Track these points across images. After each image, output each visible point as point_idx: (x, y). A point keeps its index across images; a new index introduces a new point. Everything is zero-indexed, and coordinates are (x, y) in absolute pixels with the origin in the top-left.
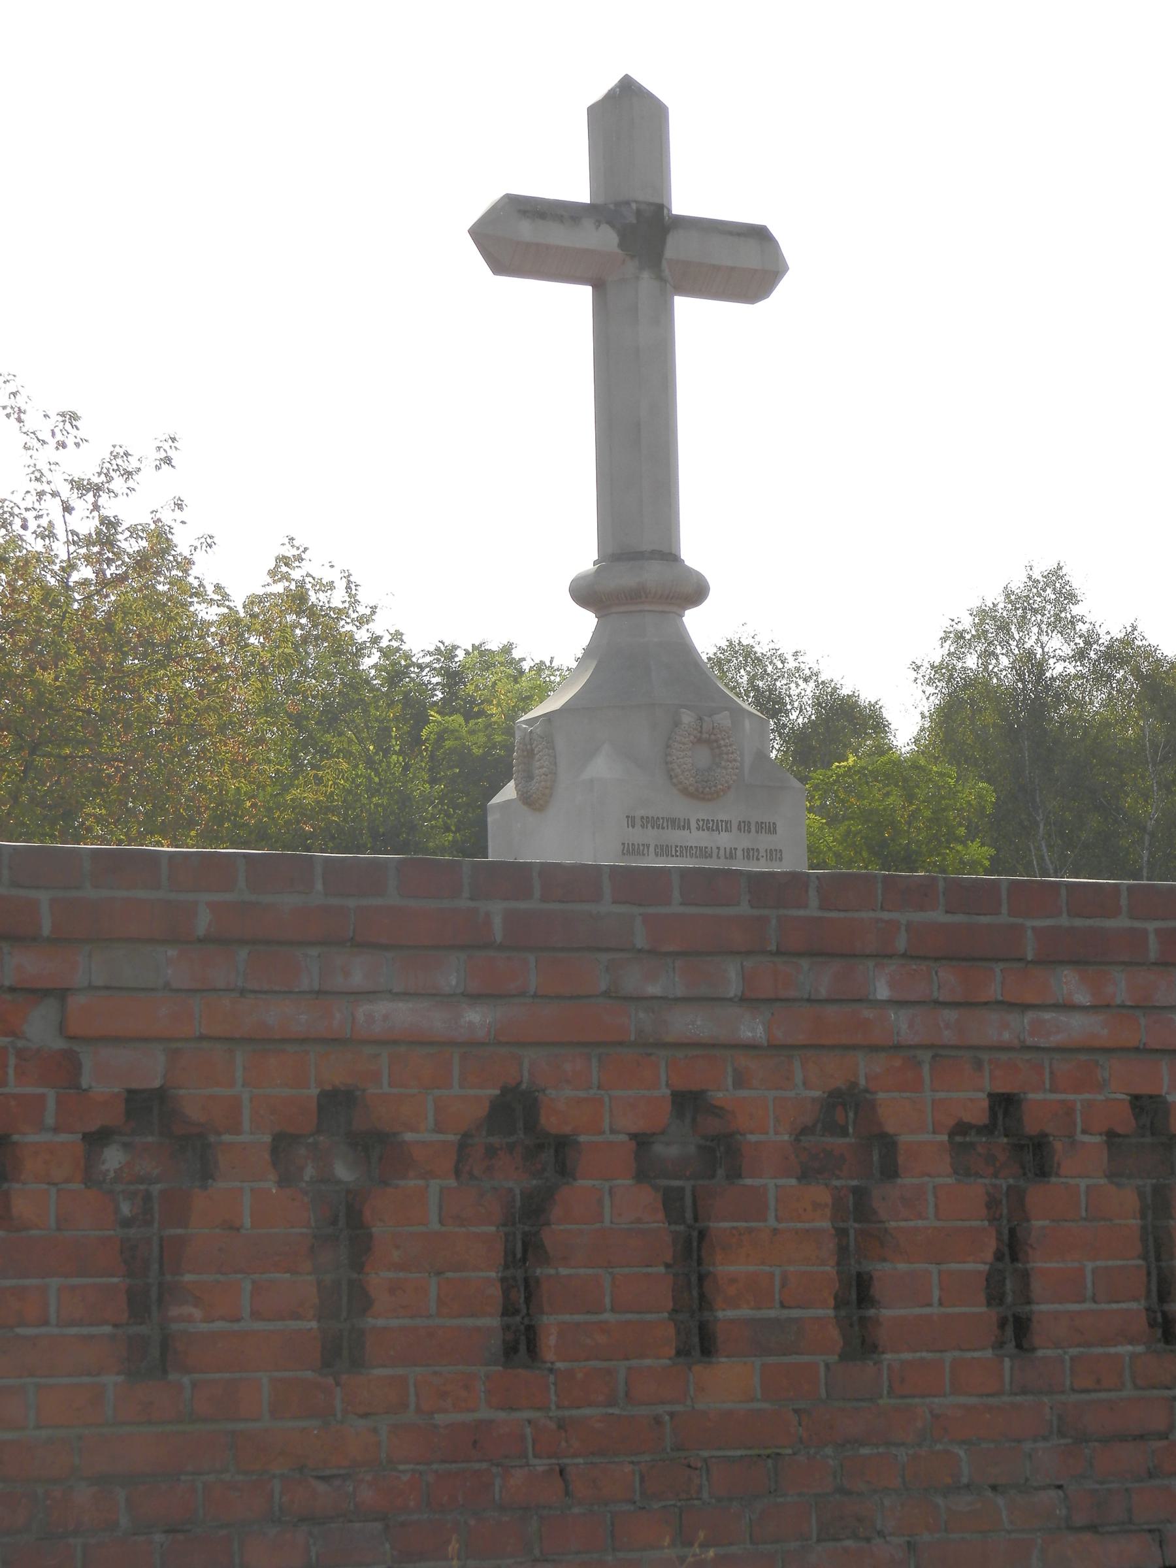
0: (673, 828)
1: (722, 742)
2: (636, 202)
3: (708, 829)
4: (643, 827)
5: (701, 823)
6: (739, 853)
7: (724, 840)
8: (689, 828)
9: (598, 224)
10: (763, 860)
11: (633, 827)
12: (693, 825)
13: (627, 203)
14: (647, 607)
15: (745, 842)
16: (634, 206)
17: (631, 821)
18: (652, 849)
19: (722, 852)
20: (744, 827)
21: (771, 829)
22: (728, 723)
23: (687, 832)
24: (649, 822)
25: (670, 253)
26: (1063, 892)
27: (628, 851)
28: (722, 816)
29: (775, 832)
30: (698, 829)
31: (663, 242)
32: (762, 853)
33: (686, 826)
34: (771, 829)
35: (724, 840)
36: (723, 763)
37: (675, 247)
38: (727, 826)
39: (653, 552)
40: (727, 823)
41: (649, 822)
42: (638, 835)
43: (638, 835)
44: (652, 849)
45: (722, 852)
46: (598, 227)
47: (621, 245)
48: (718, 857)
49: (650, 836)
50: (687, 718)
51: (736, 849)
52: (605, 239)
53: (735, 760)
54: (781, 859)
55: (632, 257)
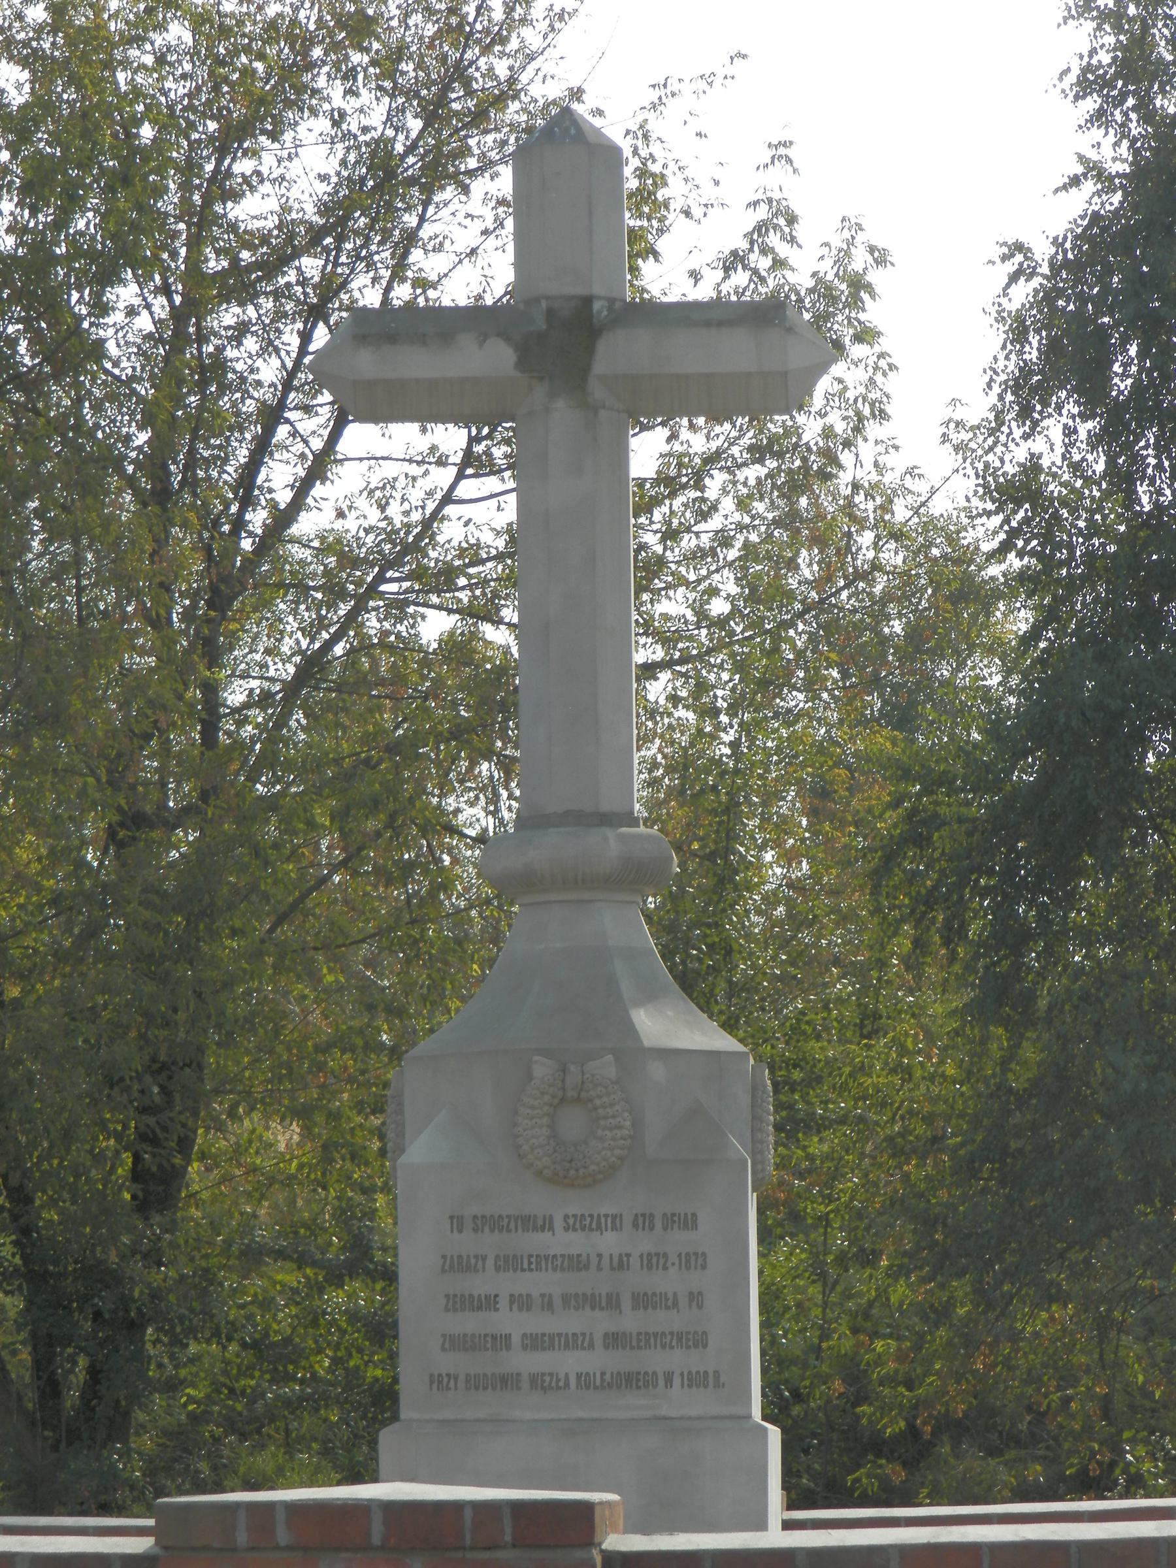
0: (526, 1229)
1: (598, 1102)
2: (547, 298)
3: (583, 1228)
4: (475, 1230)
5: (571, 1221)
6: (635, 1262)
7: (609, 1242)
8: (551, 1228)
9: (483, 339)
10: (673, 1271)
11: (460, 1231)
12: (559, 1224)
13: (537, 300)
14: (553, 897)
15: (644, 1243)
16: (544, 304)
17: (457, 1222)
18: (490, 1262)
19: (606, 1261)
20: (643, 1221)
21: (689, 1222)
22: (611, 1072)
23: (547, 1235)
24: (482, 1223)
25: (600, 367)
26: (281, 1517)
27: (452, 1266)
28: (605, 1208)
29: (695, 1226)
30: (566, 1229)
31: (591, 350)
32: (673, 1257)
33: (547, 1225)
34: (689, 1222)
35: (609, 1242)
36: (600, 1132)
37: (615, 354)
38: (615, 1222)
39: (567, 813)
40: (614, 1217)
41: (482, 1223)
42: (466, 1243)
43: (466, 1243)
44: (490, 1262)
45: (606, 1261)
46: (481, 344)
47: (523, 363)
48: (599, 1269)
49: (488, 1243)
50: (542, 1069)
51: (628, 1255)
52: (496, 358)
53: (619, 1127)
54: (704, 1267)
55: (541, 379)
